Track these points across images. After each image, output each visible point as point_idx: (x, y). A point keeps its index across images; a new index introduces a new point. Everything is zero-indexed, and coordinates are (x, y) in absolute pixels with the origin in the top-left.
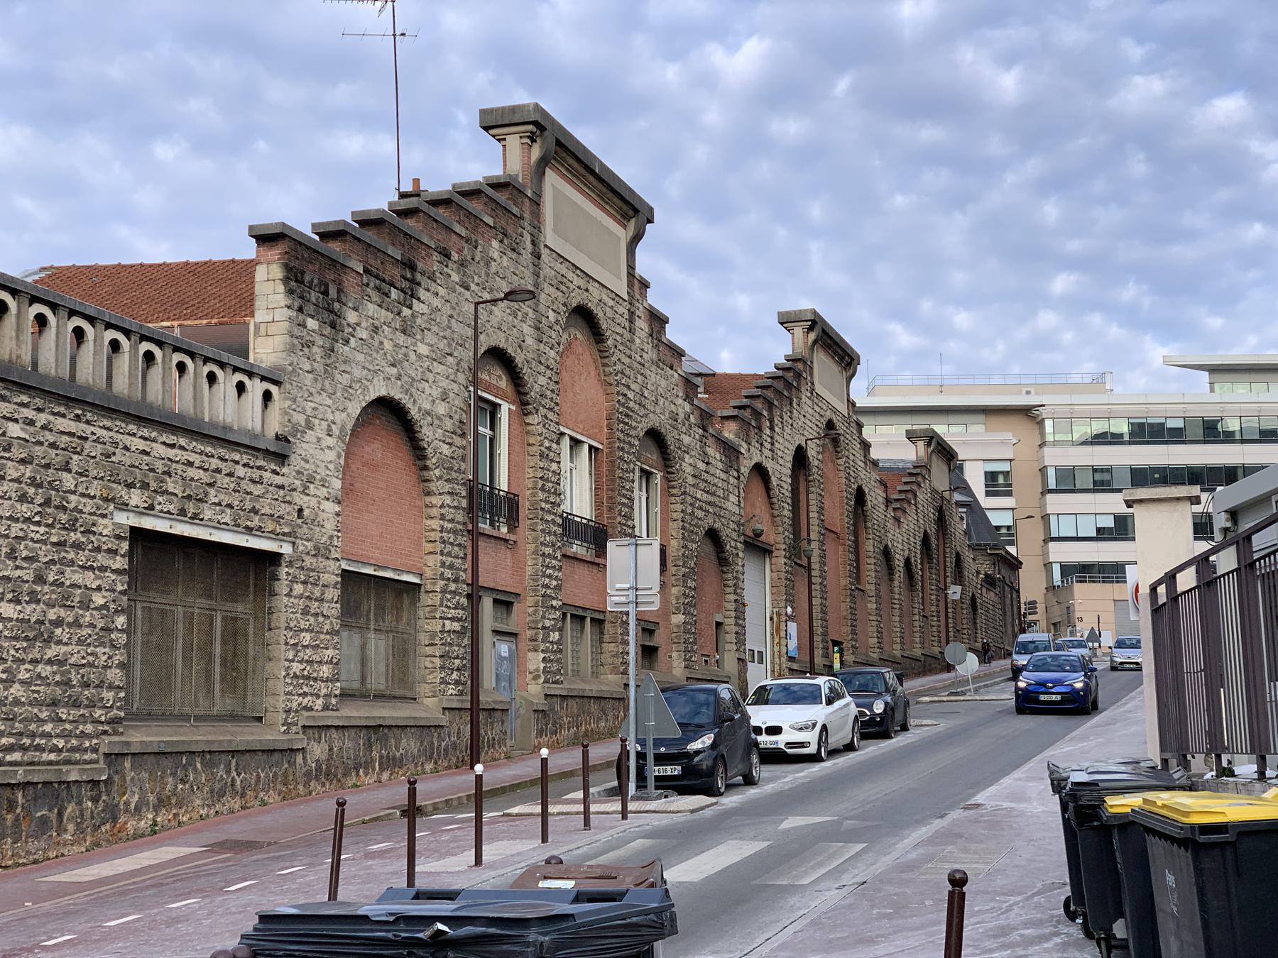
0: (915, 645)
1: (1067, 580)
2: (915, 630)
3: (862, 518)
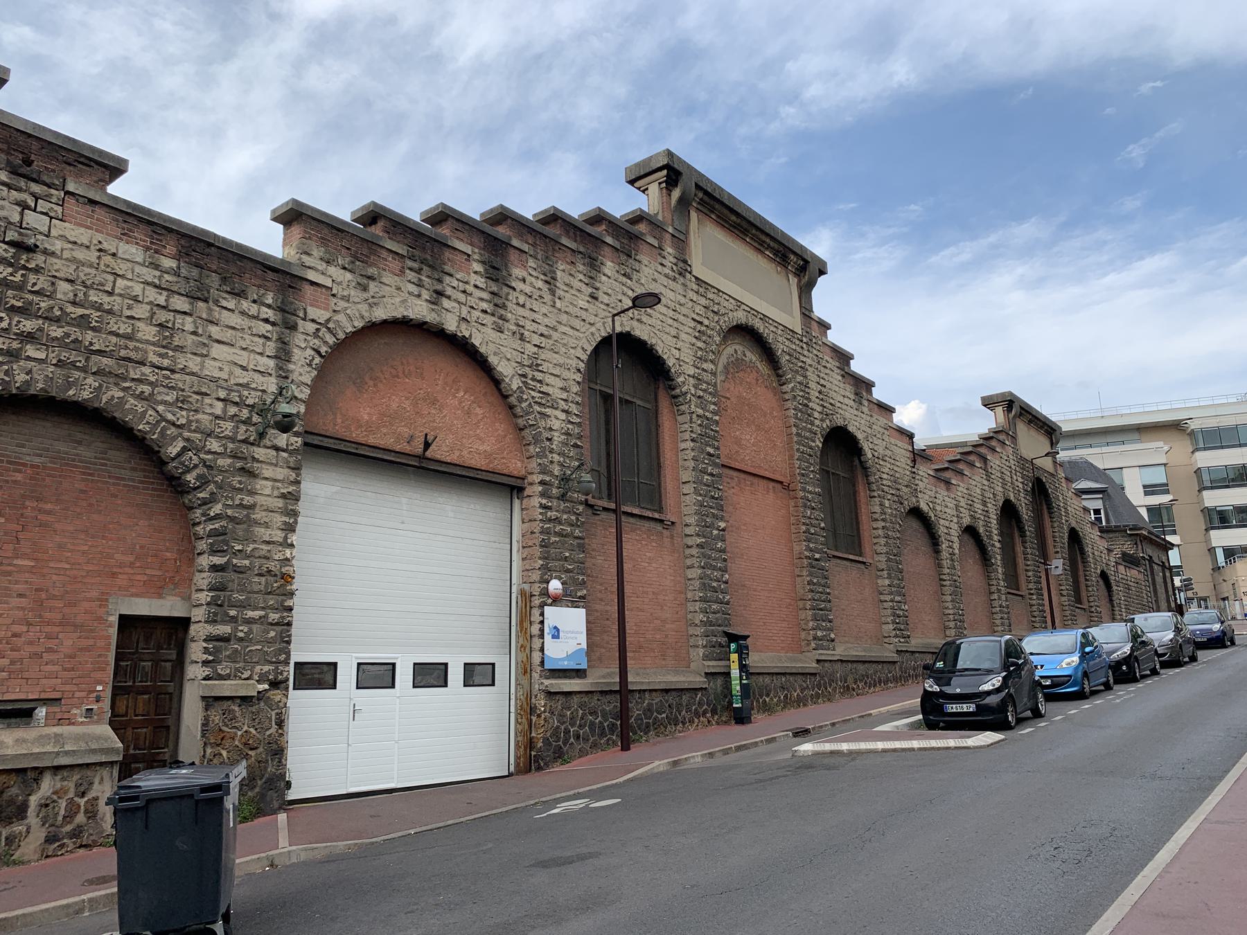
0: (996, 628)
1: (1230, 561)
2: (994, 610)
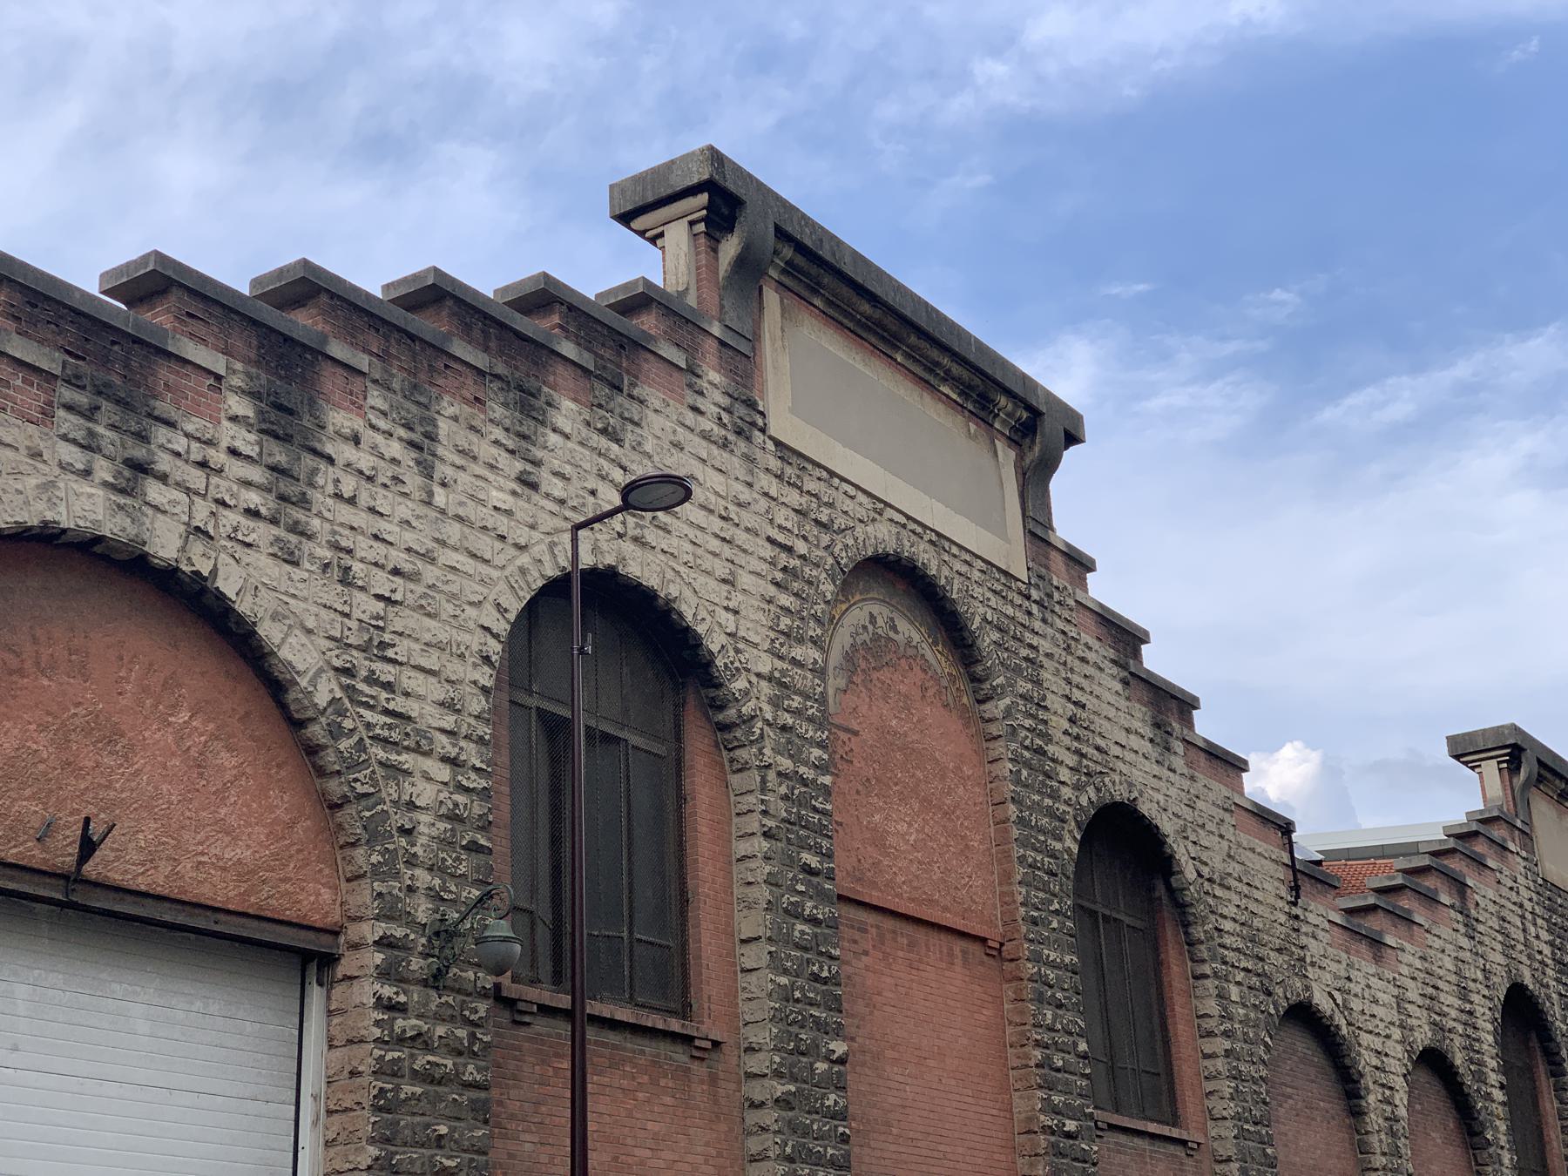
3: (1167, 912)
